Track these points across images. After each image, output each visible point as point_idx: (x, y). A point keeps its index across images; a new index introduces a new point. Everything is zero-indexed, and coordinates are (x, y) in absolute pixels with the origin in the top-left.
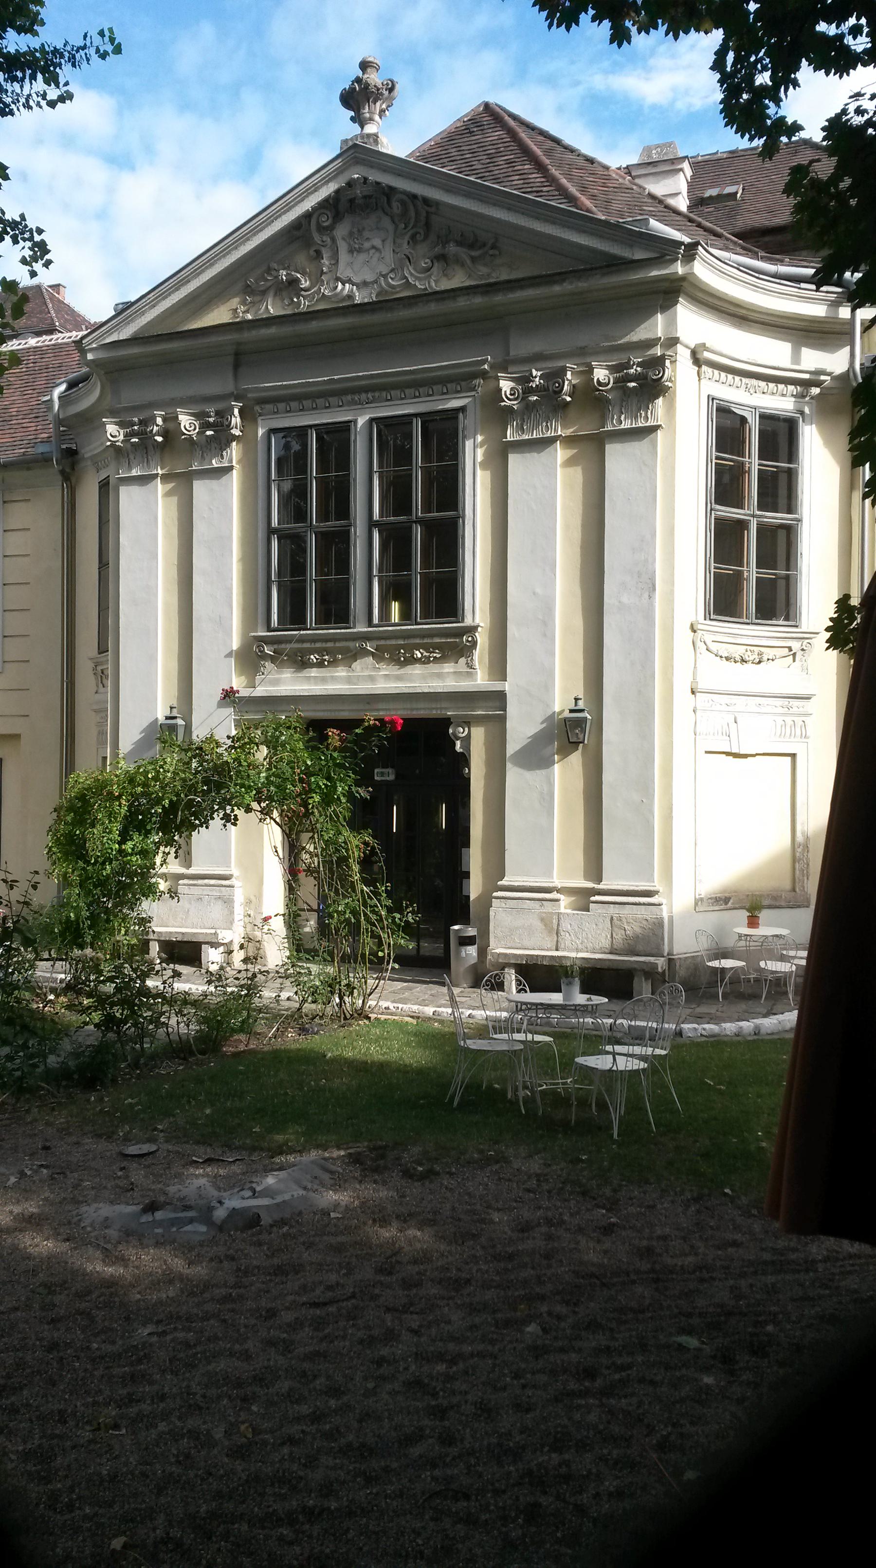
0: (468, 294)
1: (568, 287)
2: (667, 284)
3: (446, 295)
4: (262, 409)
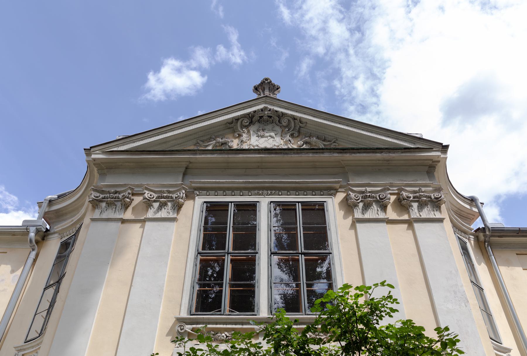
2: (431, 162)
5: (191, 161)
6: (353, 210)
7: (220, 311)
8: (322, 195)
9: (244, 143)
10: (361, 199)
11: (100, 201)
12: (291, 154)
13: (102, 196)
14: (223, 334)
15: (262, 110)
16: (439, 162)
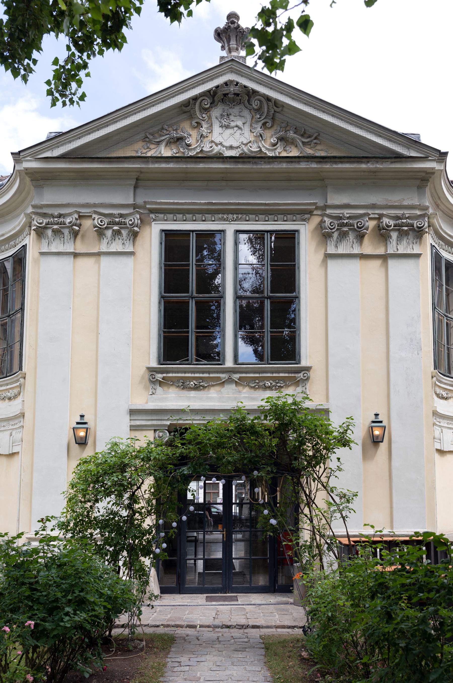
0: (308, 161)
1: (371, 166)
2: (423, 174)
3: (293, 160)
4: (156, 217)
5: (142, 170)
6: (327, 242)
7: (188, 360)
8: (294, 221)
9: (204, 137)
10: (336, 227)
11: (45, 228)
12: (261, 164)
13: (45, 221)
14: (192, 383)
15: (226, 84)
16: (433, 173)
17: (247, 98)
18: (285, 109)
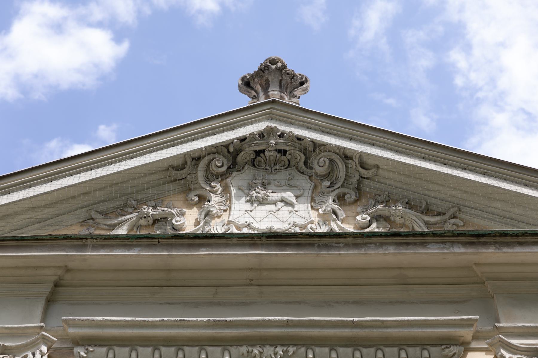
5: (71, 265)
17: (303, 157)
18: (381, 172)
